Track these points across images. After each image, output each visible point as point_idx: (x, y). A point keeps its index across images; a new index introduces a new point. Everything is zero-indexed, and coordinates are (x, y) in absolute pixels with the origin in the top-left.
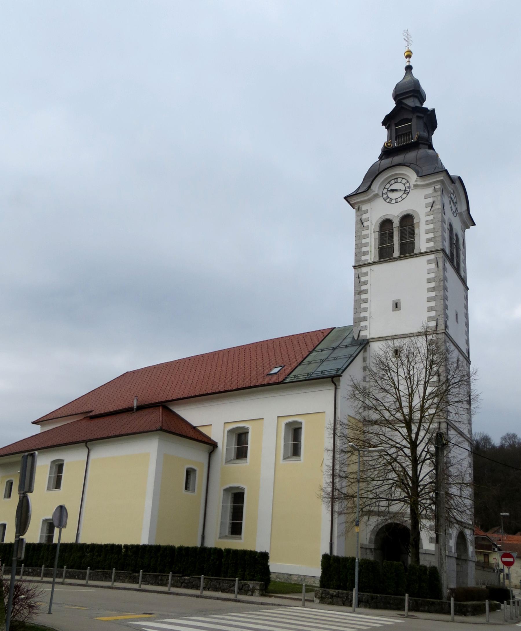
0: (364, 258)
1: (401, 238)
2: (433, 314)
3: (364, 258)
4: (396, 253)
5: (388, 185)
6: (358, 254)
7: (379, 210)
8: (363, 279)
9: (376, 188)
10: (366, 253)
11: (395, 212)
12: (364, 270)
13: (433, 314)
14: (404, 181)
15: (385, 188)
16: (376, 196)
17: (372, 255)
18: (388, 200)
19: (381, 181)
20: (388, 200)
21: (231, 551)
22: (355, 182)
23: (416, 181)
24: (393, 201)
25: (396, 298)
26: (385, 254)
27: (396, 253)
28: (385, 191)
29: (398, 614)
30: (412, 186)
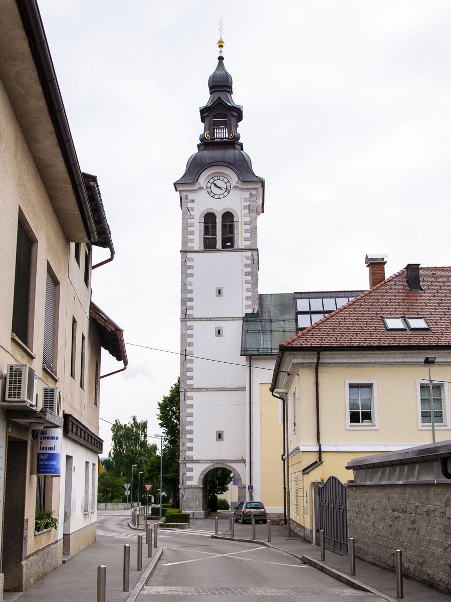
0: (190, 245)
1: (223, 233)
2: (188, 402)
3: (190, 245)
4: (219, 245)
5: (216, 178)
6: (185, 242)
7: (205, 201)
8: (189, 263)
9: (203, 180)
10: (192, 241)
11: (219, 207)
12: (189, 255)
13: (188, 402)
14: (226, 180)
15: (208, 182)
16: (201, 188)
17: (197, 242)
18: (212, 194)
19: (209, 174)
20: (212, 194)
21: (103, 488)
22: (180, 171)
23: (236, 183)
24: (216, 197)
25: (219, 286)
26: (209, 245)
27: (219, 245)
28: (212, 181)
29: (306, 493)
30: (232, 186)
